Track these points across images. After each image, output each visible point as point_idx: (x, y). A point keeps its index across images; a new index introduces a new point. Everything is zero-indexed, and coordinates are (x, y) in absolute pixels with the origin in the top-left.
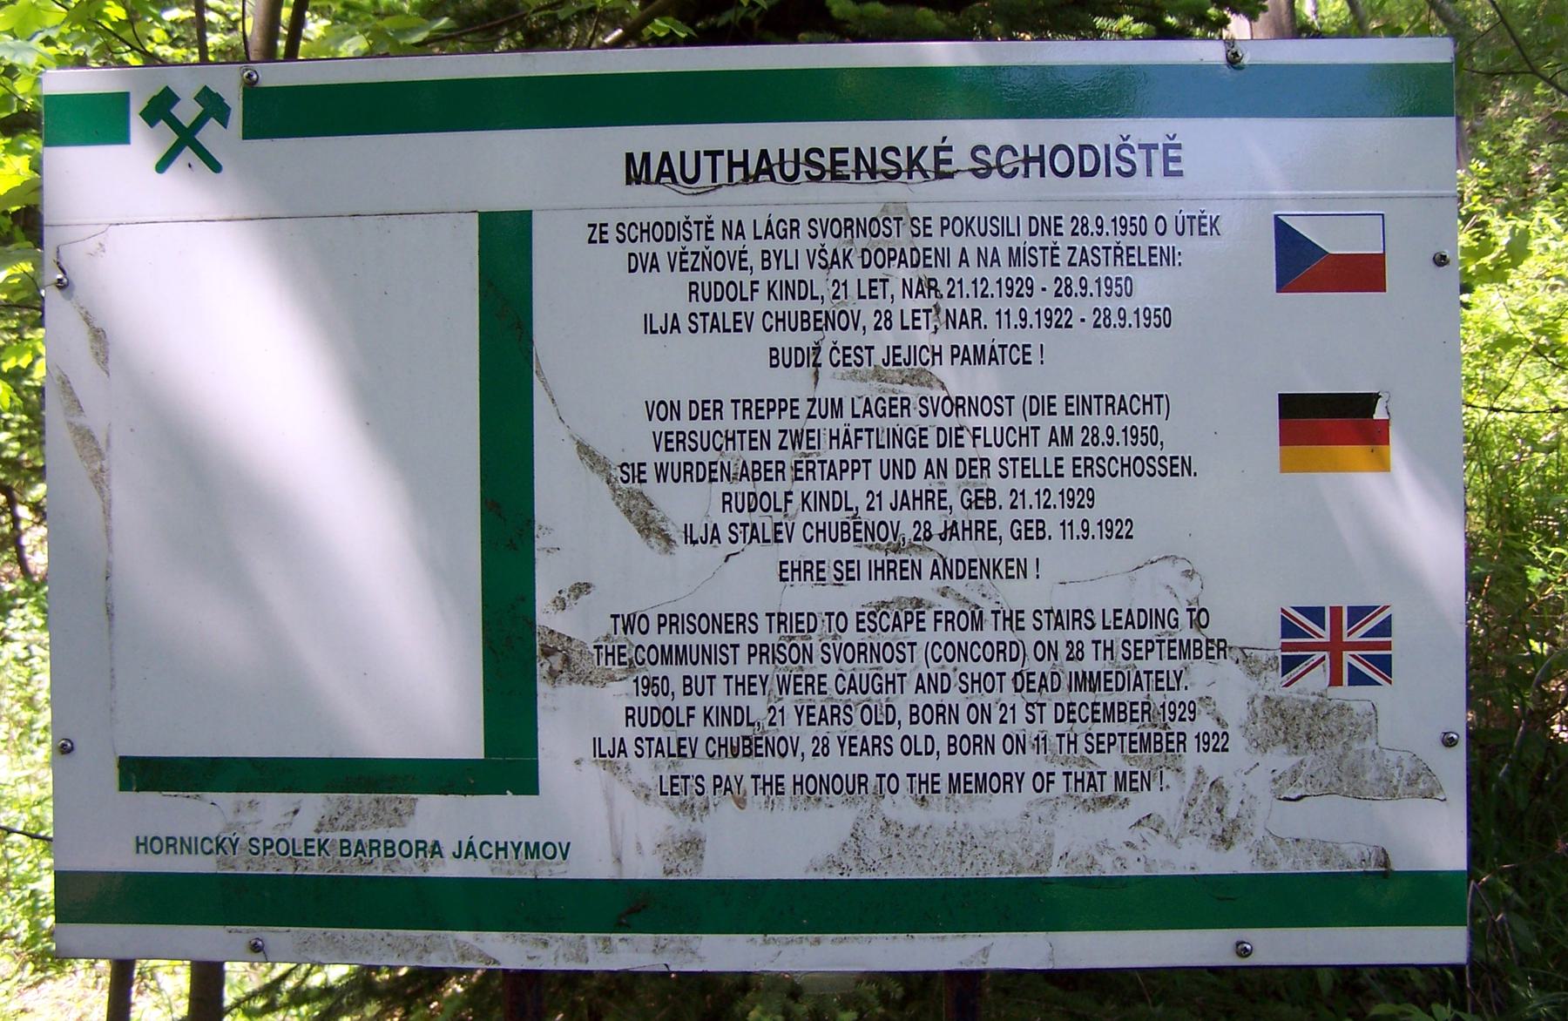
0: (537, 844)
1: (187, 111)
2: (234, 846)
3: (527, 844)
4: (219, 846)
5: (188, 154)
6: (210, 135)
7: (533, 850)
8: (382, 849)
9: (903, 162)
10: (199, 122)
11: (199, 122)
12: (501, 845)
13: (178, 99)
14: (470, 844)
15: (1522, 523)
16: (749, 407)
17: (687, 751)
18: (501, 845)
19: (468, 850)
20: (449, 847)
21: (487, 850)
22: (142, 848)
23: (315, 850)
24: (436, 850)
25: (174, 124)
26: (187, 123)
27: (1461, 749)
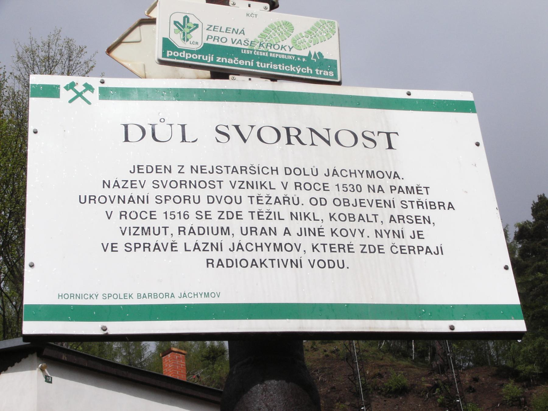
0: (208, 293)
1: (80, 88)
2: (97, 296)
3: (205, 293)
4: (91, 296)
6: (87, 95)
7: (207, 295)
8: (153, 296)
10: (76, 91)
12: (196, 294)
14: (185, 293)
18: (196, 294)
19: (105, 297)
20: (177, 295)
22: (60, 297)
23: (128, 297)
24: (173, 296)
27: (450, 331)
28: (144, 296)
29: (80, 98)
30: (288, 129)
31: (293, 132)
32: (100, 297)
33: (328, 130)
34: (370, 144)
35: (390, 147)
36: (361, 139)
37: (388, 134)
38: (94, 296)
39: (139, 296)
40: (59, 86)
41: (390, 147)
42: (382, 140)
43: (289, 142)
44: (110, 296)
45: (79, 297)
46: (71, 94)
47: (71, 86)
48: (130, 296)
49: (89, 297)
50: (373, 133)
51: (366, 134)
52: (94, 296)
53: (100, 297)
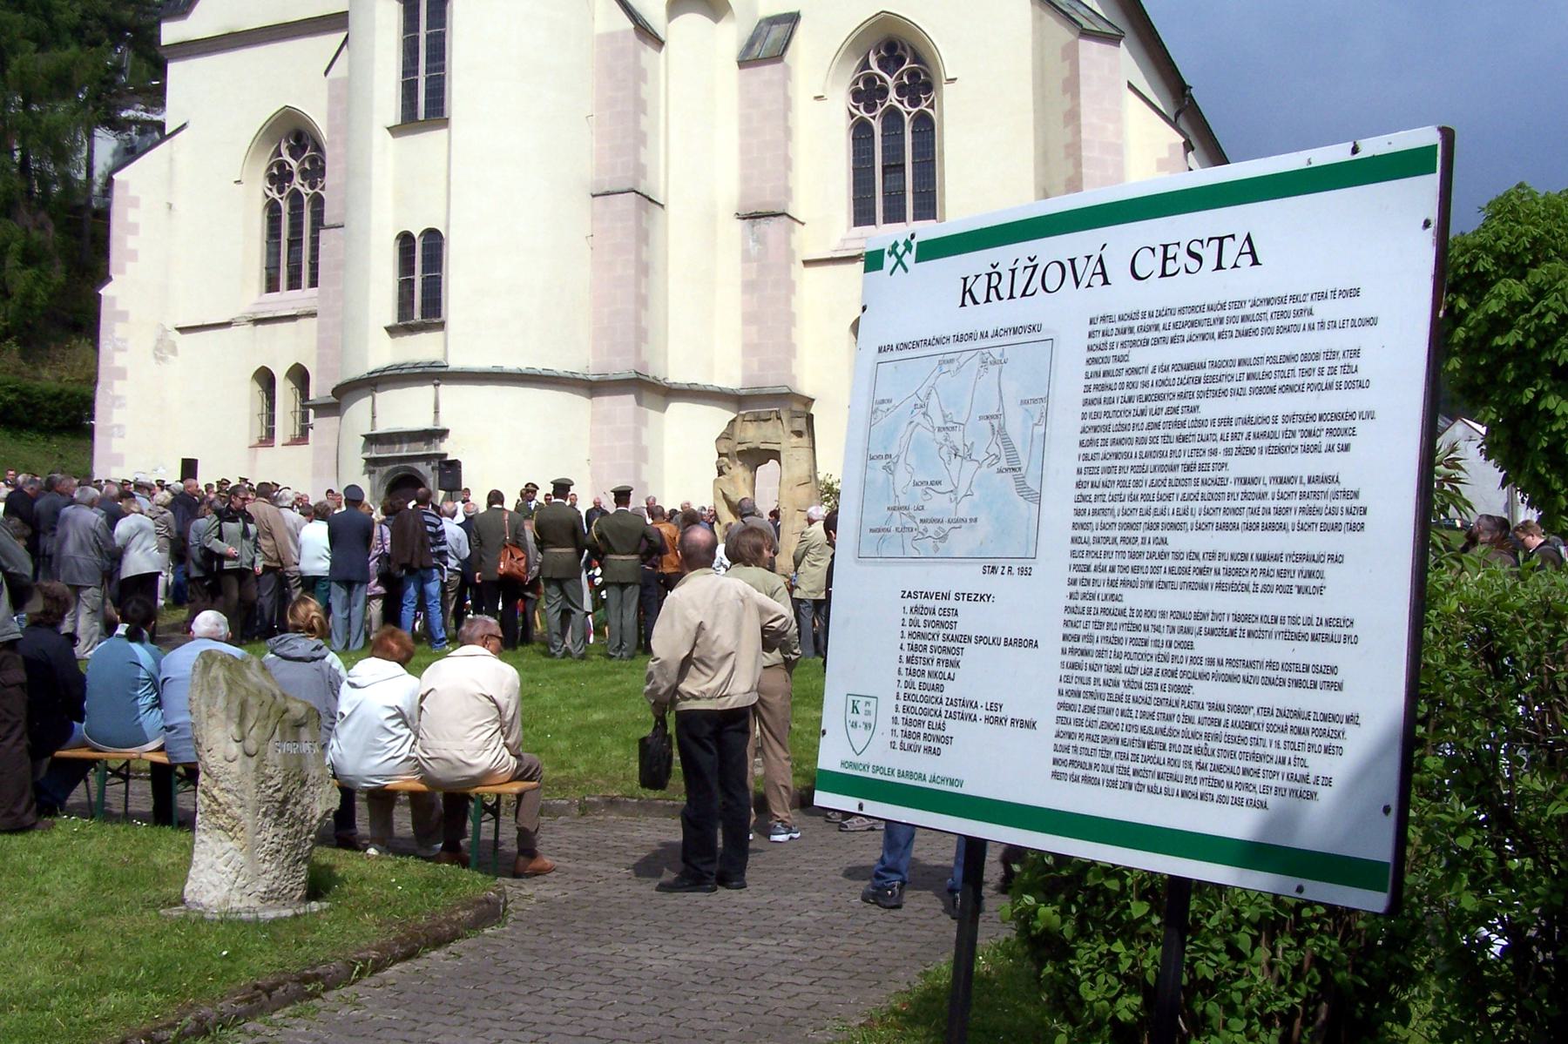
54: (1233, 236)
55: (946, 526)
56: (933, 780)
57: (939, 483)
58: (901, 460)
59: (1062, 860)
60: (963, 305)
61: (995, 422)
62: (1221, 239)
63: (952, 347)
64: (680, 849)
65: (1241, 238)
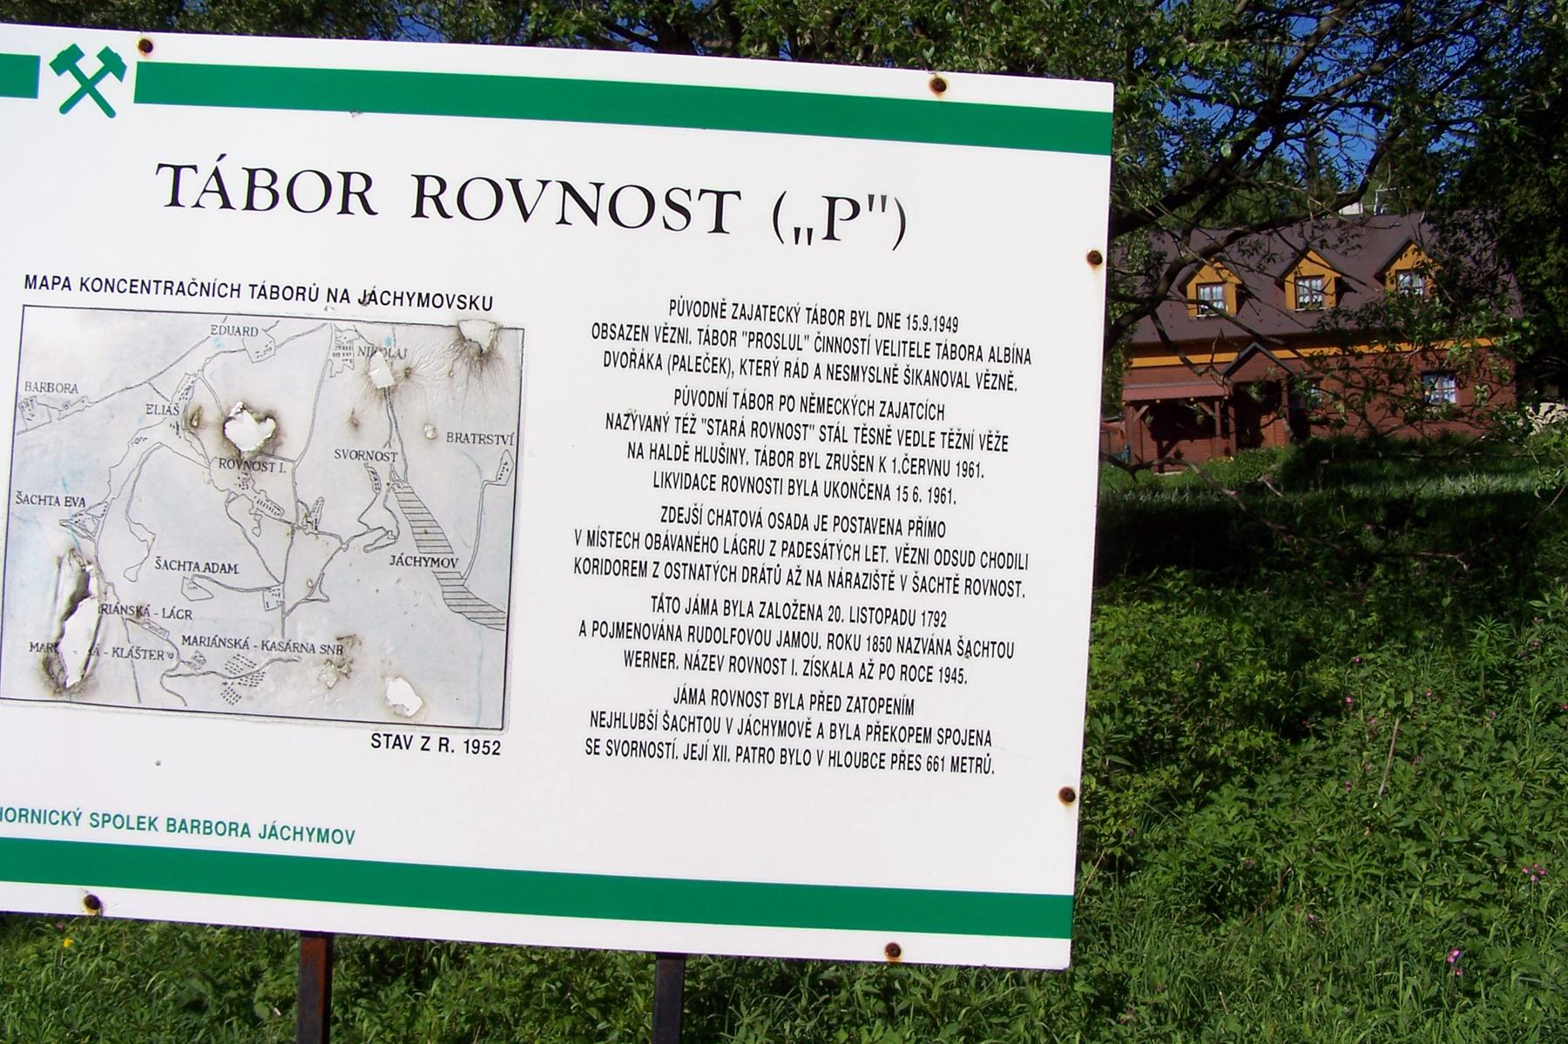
4: (64, 818)
5: (88, 98)
6: (108, 86)
7: (323, 836)
9: (468, 301)
10: (100, 75)
11: (100, 75)
13: (74, 46)
15: (1504, 429)
16: (960, 381)
17: (715, 666)
20: (256, 829)
21: (286, 833)
23: (146, 826)
24: (246, 831)
25: (79, 75)
26: (89, 75)
28: (183, 827)
29: (79, 86)
30: (347, 176)
31: (357, 184)
32: (85, 820)
33: (598, 186)
34: (676, 219)
35: (719, 228)
36: (661, 207)
37: (720, 196)
38: (71, 818)
39: (171, 824)
40: (35, 60)
41: (719, 228)
42: (703, 211)
43: (345, 210)
44: (107, 818)
45: (38, 817)
46: (69, 84)
47: (67, 61)
48: (151, 824)
49: (60, 818)
50: (688, 192)
51: (674, 197)
52: (71, 818)
53: (85, 820)
54: (194, 168)
55: (261, 658)
56: (272, 832)
57: (233, 569)
58: (120, 506)
59: (588, 959)
60: (419, 213)
61: (382, 468)
62: (177, 169)
63: (245, 303)
64: (1110, 124)
65: (206, 171)
